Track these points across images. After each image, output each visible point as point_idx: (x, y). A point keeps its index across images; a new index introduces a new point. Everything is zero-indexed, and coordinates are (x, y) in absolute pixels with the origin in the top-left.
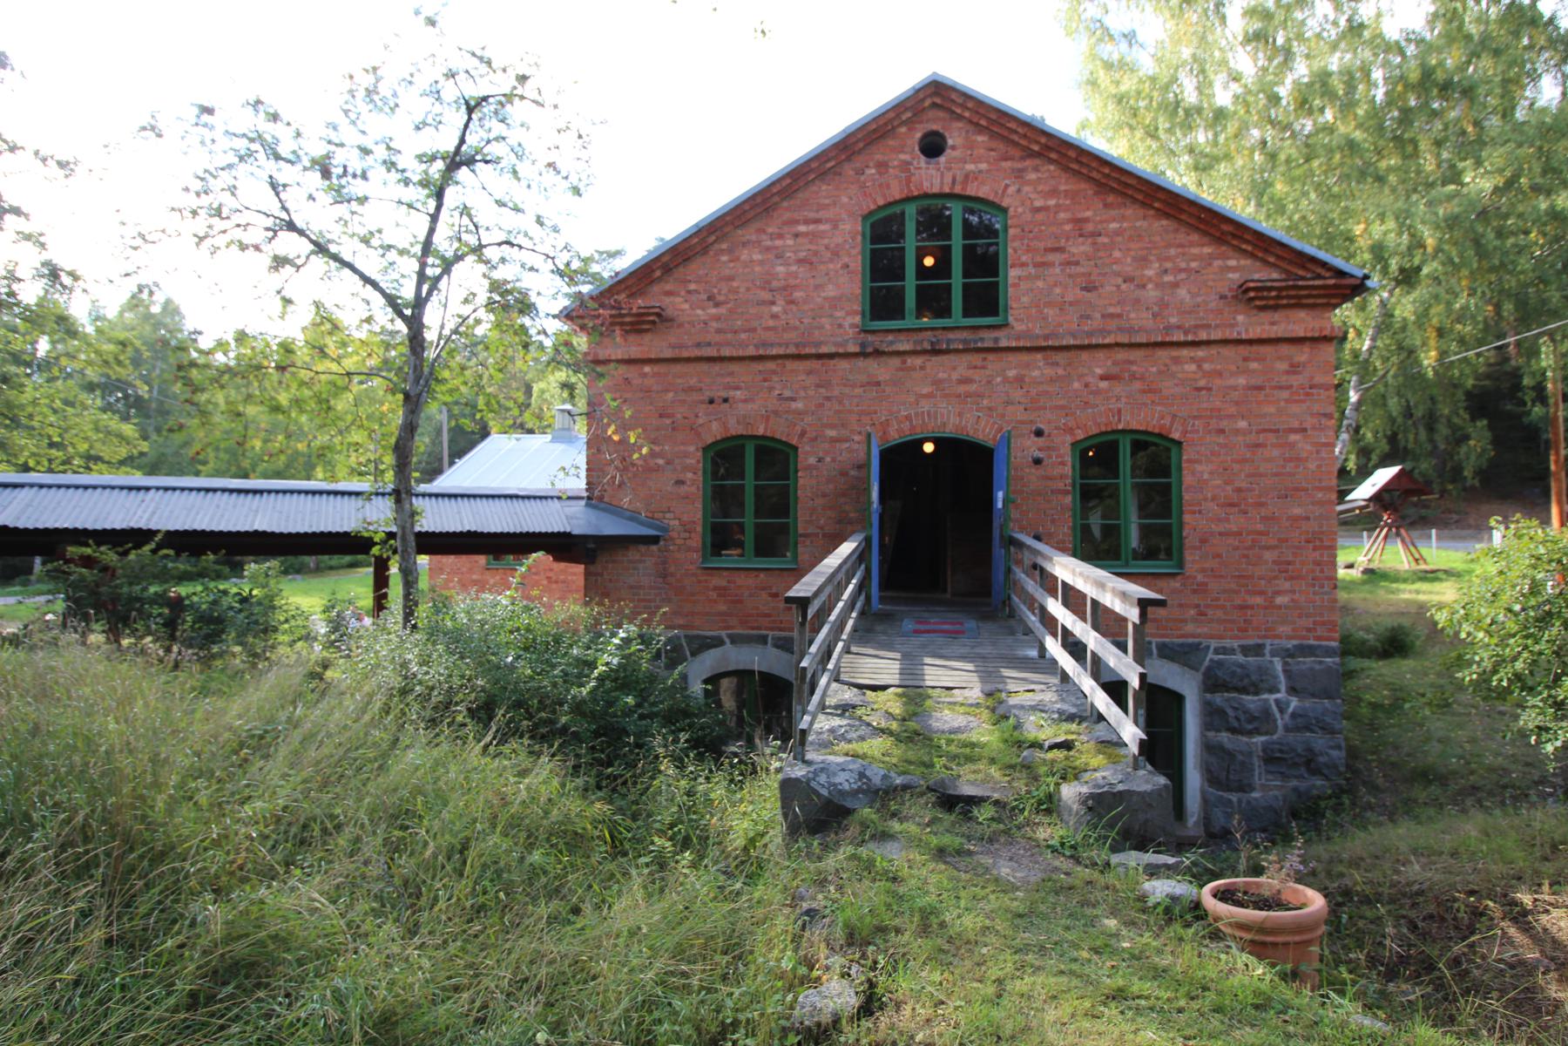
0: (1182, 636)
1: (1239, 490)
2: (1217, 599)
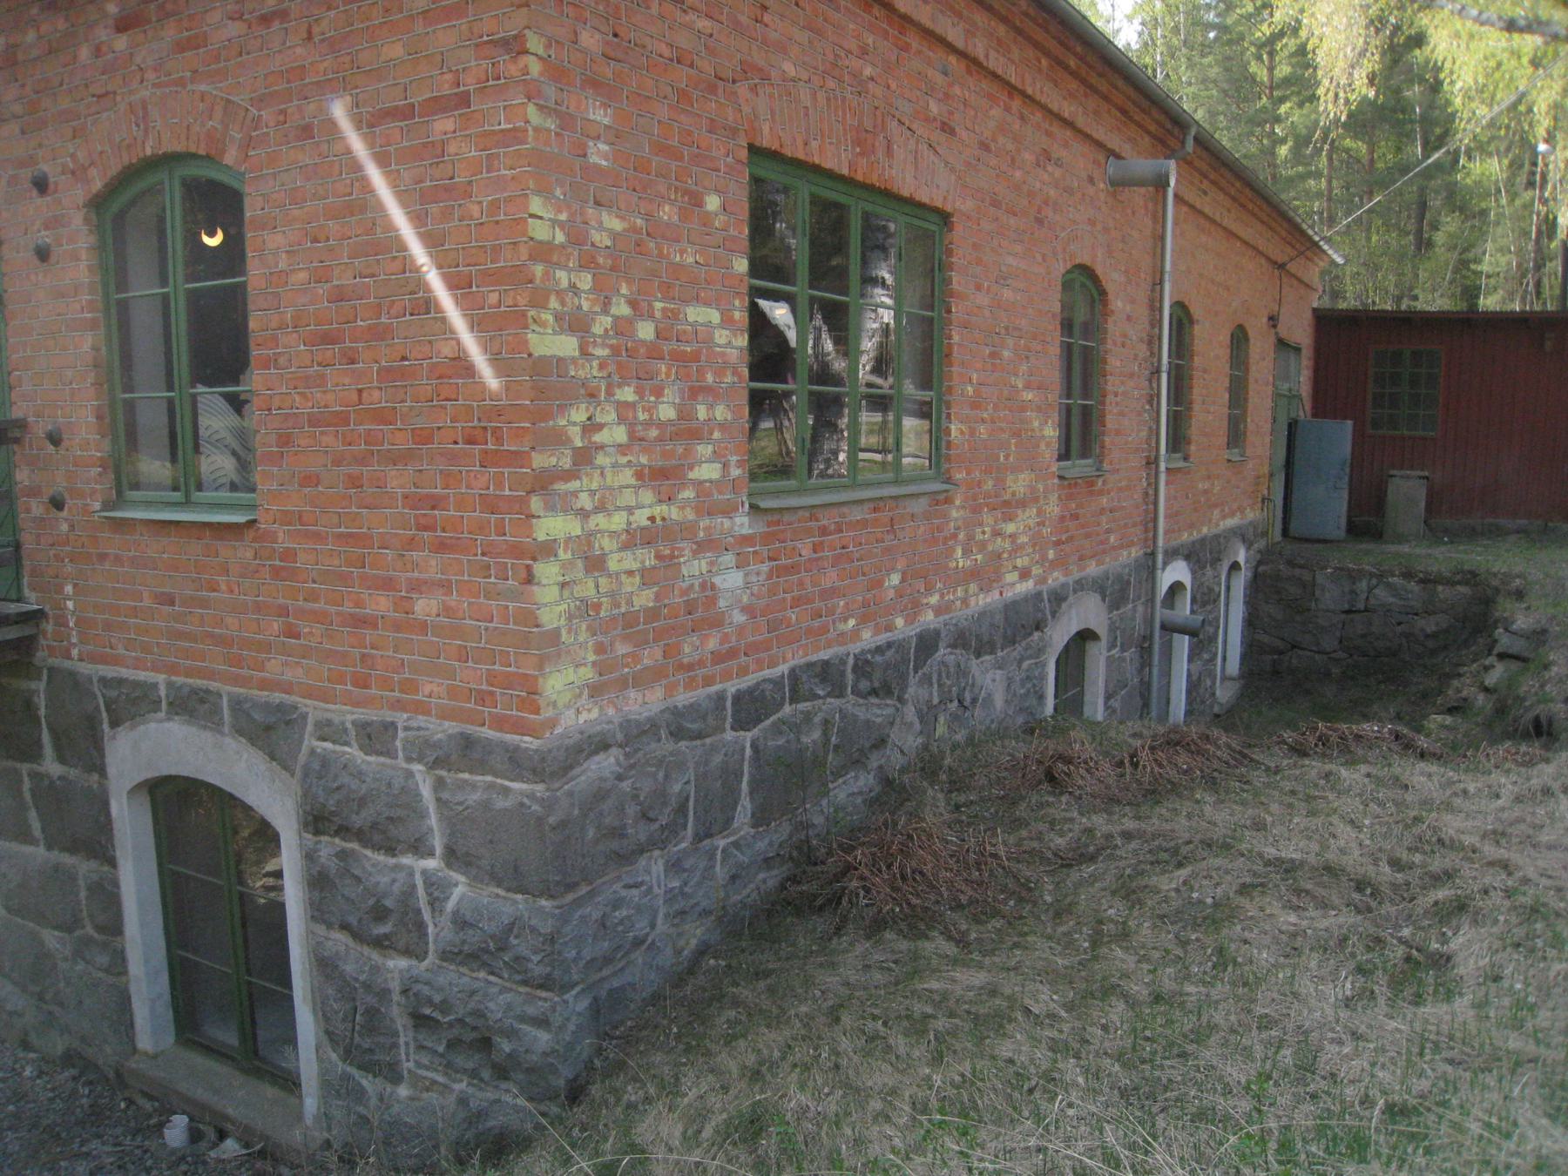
0: (264, 685)
1: (339, 296)
2: (312, 596)
